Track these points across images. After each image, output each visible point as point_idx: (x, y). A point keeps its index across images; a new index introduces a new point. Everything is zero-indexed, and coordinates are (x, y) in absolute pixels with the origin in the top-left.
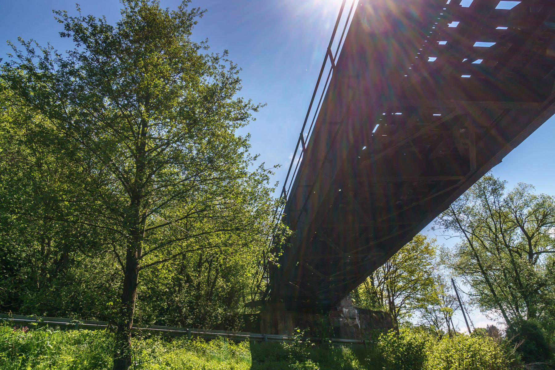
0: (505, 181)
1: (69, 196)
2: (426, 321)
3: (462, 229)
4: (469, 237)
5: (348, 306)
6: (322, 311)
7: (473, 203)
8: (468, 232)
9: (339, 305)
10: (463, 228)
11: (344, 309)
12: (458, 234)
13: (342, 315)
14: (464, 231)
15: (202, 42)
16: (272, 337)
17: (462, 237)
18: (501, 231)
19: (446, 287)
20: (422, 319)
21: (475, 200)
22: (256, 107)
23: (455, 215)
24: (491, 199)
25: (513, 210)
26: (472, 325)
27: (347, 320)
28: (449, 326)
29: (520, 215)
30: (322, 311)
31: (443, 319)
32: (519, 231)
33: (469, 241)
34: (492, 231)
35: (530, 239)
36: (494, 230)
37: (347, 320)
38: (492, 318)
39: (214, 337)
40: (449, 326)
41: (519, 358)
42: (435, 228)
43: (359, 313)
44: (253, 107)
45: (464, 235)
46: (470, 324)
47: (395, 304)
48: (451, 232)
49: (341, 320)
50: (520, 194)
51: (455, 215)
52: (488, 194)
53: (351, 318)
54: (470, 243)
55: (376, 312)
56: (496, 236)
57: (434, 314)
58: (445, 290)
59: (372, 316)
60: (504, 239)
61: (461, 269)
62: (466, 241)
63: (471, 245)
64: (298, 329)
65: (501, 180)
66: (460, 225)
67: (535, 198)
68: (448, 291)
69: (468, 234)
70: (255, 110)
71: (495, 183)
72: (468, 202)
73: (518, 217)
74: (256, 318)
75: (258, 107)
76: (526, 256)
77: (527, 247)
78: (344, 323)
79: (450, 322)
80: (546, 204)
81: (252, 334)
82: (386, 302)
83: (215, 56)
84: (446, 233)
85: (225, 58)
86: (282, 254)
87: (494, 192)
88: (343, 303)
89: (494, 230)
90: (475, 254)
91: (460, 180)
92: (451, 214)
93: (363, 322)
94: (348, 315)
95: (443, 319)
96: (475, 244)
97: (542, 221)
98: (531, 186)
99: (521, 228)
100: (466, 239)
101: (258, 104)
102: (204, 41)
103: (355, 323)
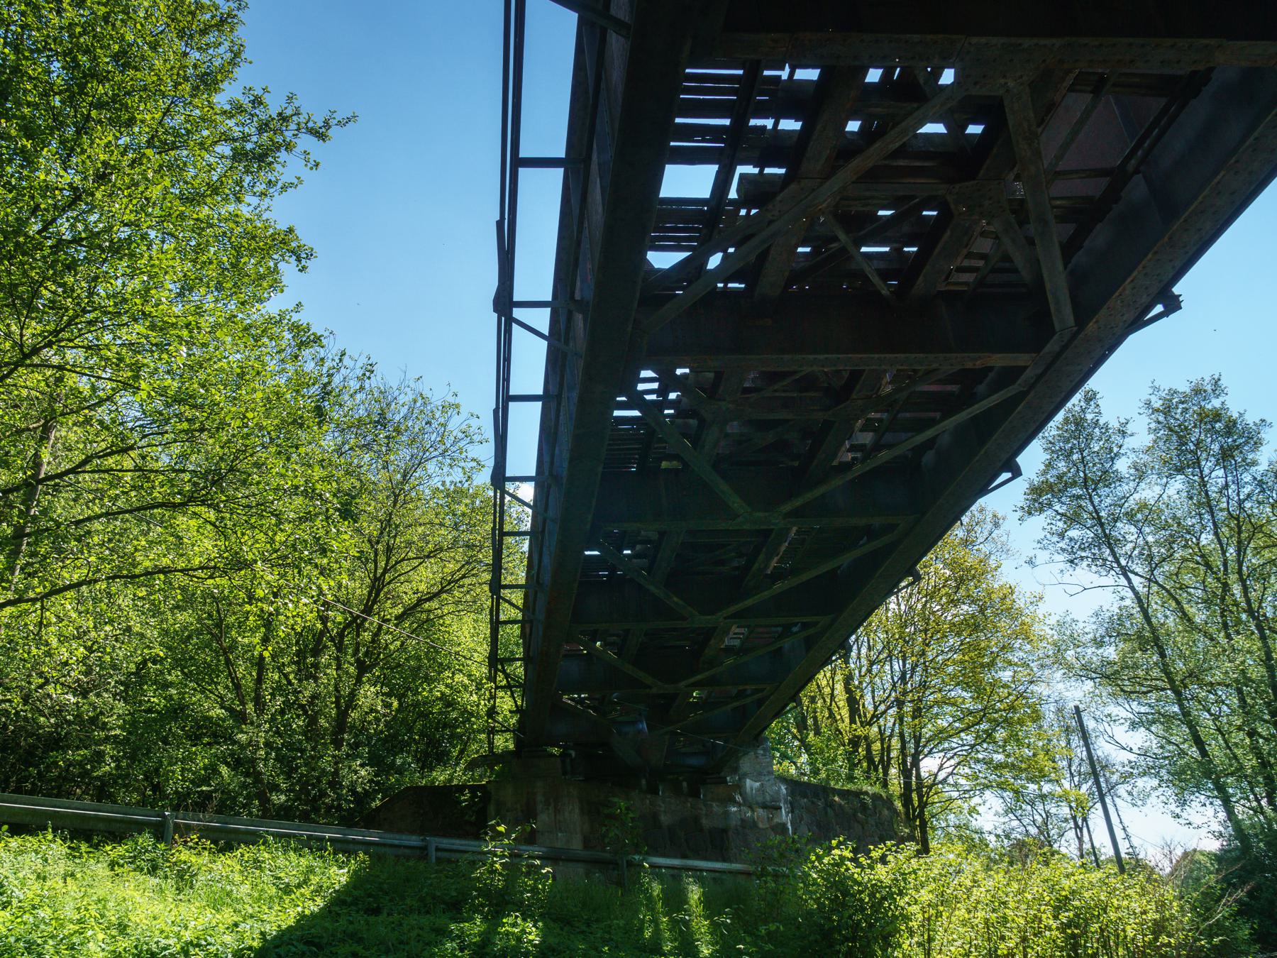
0: (1263, 421)
1: (247, 510)
2: (1015, 823)
4: (1140, 589)
5: (760, 774)
6: (685, 784)
7: (1158, 490)
8: (1136, 574)
9: (735, 770)
10: (1123, 562)
11: (748, 782)
12: (1110, 579)
13: (738, 798)
14: (1125, 572)
16: (455, 847)
18: (1240, 572)
20: (1007, 819)
21: (1165, 480)
23: (1102, 525)
24: (1217, 477)
26: (1128, 837)
27: (753, 811)
28: (1080, 839)
30: (685, 784)
31: (1066, 820)
37: (753, 811)
38: (1191, 819)
39: (252, 839)
40: (1080, 839)
41: (1245, 933)
42: (1038, 562)
43: (792, 793)
44: (310, 125)
45: (1126, 583)
46: (1119, 834)
48: (1085, 574)
49: (734, 809)
51: (1102, 525)
52: (1207, 466)
53: (764, 807)
54: (1141, 606)
55: (844, 794)
59: (831, 804)
63: (1144, 611)
64: (499, 825)
65: (1251, 419)
66: (1113, 553)
69: (1136, 581)
70: (320, 135)
71: (1231, 427)
72: (1142, 485)
74: (477, 797)
78: (742, 820)
79: (1085, 830)
81: (387, 835)
84: (1067, 579)
87: (1226, 456)
88: (746, 764)
90: (1151, 639)
92: (1089, 523)
93: (801, 819)
94: (760, 799)
95: (1066, 820)
100: (1130, 594)
101: (327, 114)
103: (776, 820)
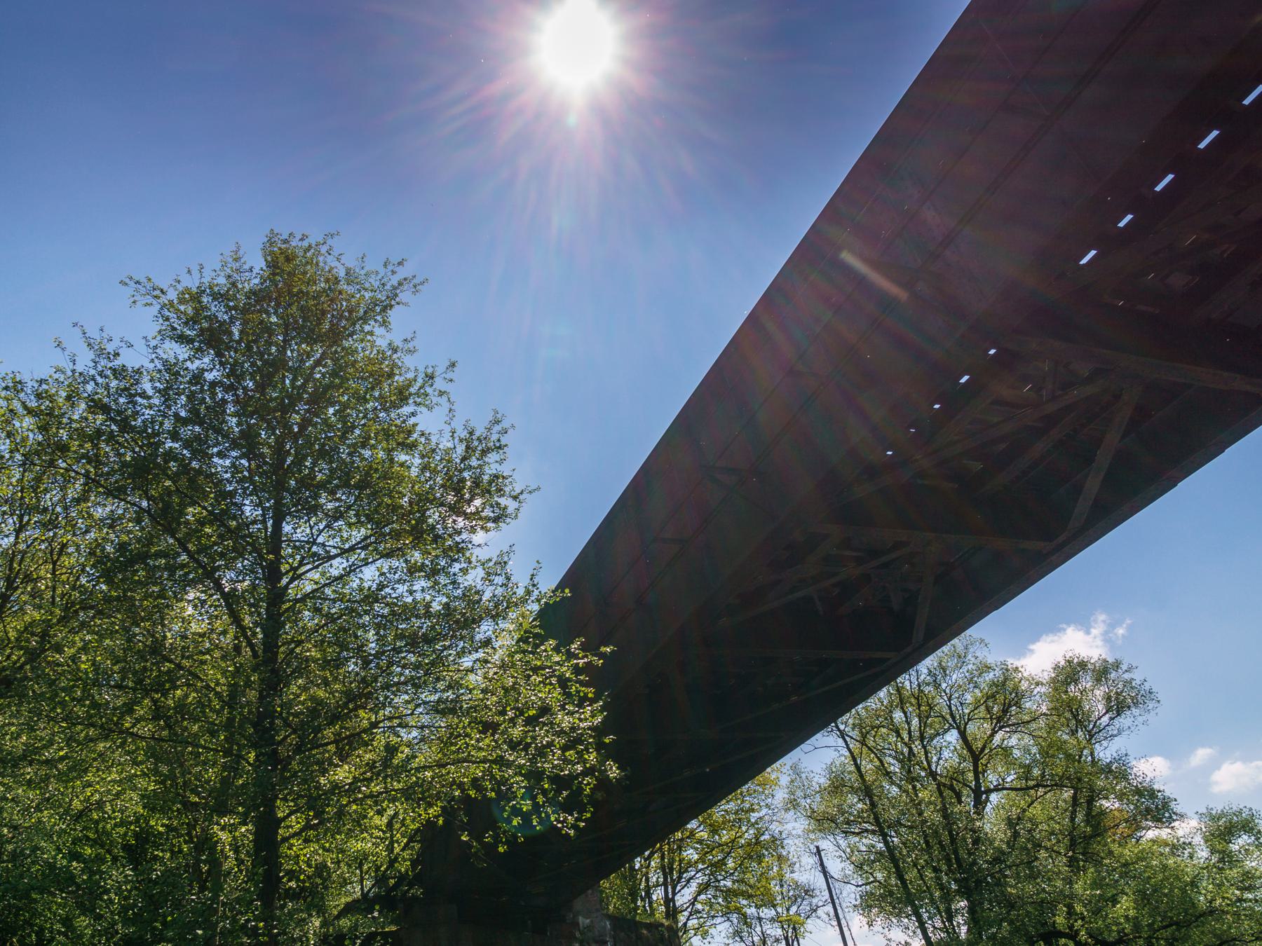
3: (839, 730)
6: (529, 922)
11: (581, 919)
15: (406, 340)
17: (839, 749)
19: (789, 863)
22: (518, 491)
25: (945, 692)
29: (958, 704)
30: (529, 922)
32: (953, 736)
33: (854, 759)
34: (902, 739)
35: (976, 757)
36: (905, 736)
43: (614, 927)
47: (678, 904)
50: (960, 657)
56: (911, 750)
57: (758, 929)
58: (786, 869)
60: (927, 757)
61: (824, 822)
62: (848, 760)
67: (988, 668)
68: (792, 872)
73: (954, 708)
75: (522, 493)
76: (968, 799)
77: (970, 776)
80: (1010, 685)
82: (658, 894)
83: (430, 371)
85: (450, 375)
86: (589, 815)
88: (578, 904)
89: (905, 736)
91: (889, 659)
96: (868, 766)
97: (999, 719)
98: (982, 641)
99: (960, 732)
102: (409, 339)
